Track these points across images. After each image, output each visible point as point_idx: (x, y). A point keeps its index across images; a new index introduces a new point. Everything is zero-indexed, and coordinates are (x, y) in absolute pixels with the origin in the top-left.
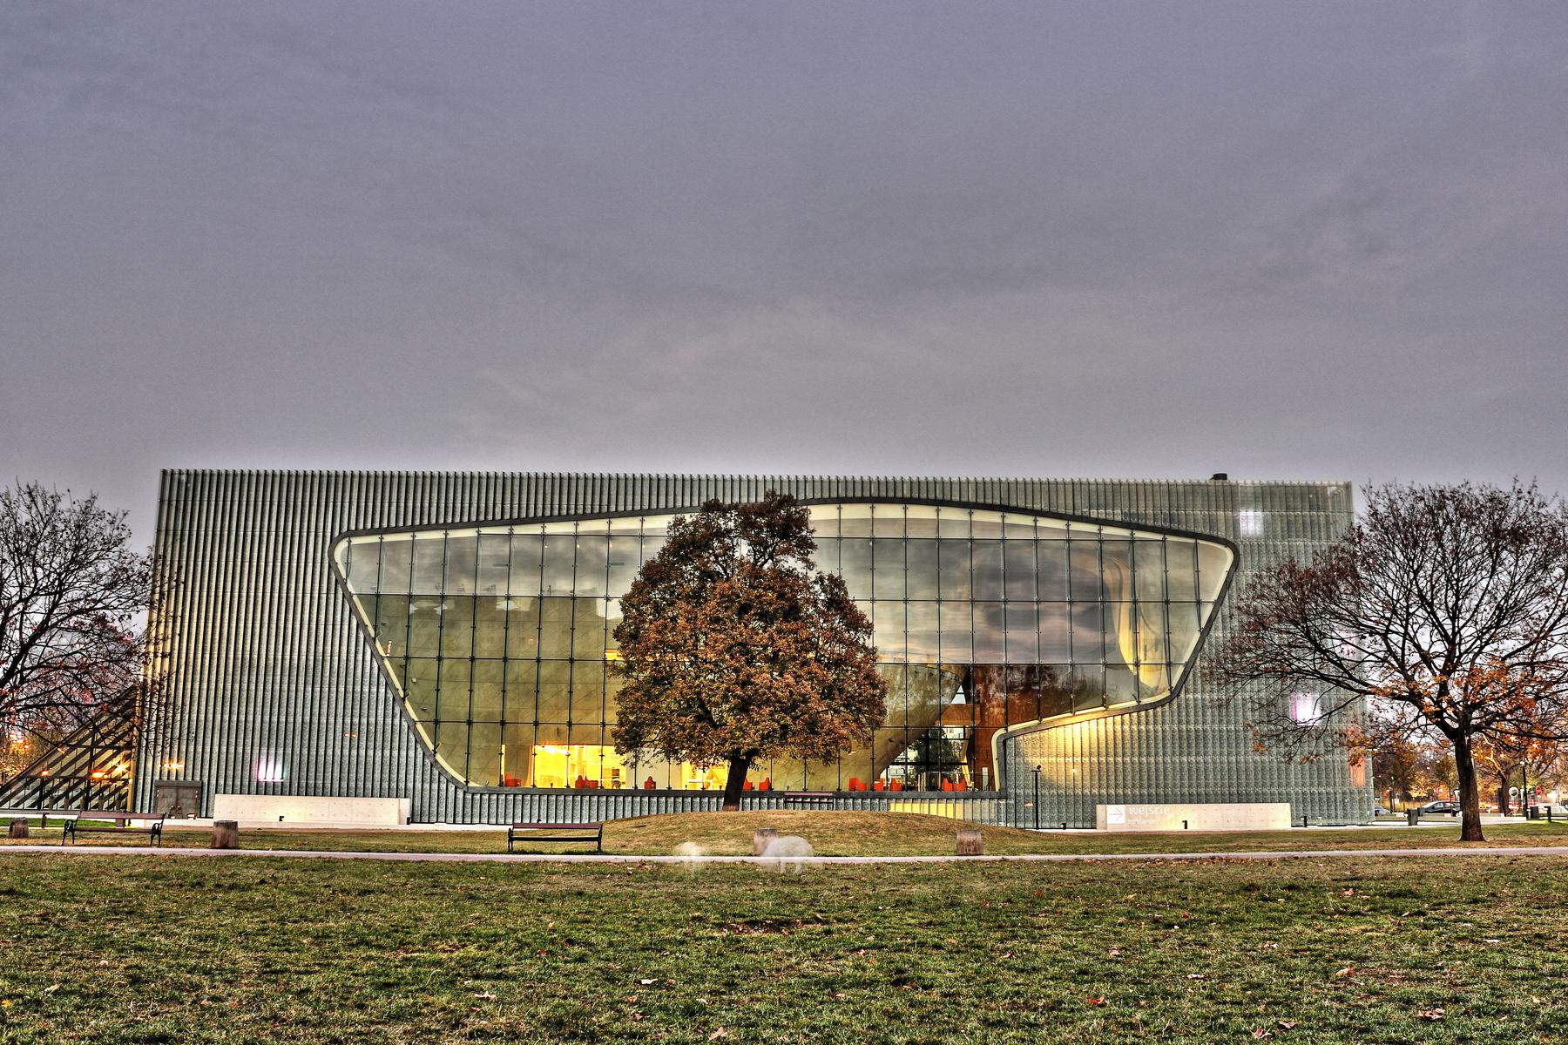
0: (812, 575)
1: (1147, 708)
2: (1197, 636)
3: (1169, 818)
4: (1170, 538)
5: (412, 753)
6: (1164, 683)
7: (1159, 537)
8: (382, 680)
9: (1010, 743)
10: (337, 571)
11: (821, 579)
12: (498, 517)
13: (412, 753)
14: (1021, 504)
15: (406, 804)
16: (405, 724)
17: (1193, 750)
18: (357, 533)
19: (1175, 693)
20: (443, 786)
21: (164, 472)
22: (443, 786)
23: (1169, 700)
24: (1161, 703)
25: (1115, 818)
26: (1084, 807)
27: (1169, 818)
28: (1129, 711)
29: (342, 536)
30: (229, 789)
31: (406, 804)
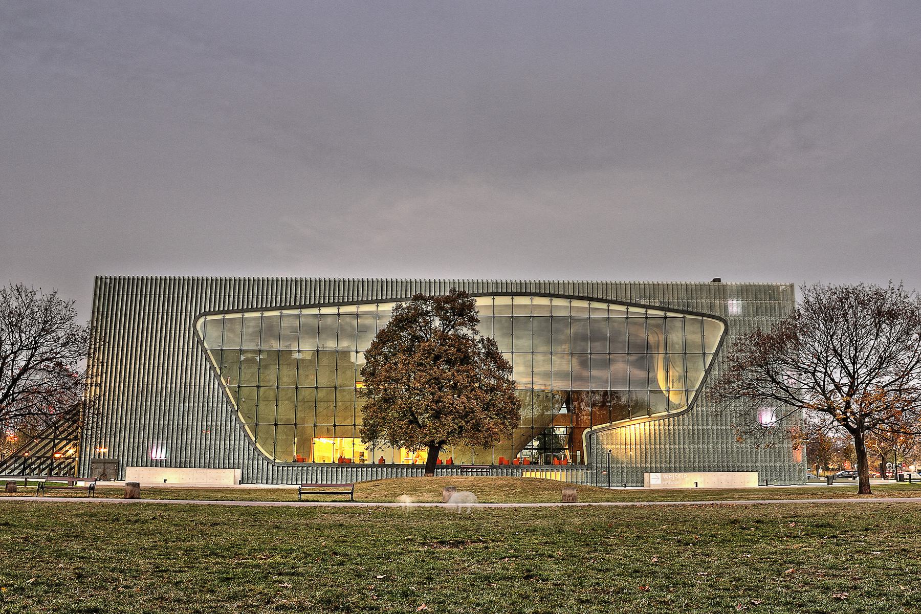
0: (477, 338)
2: (704, 373)
5: (242, 443)
6: (684, 401)
7: (681, 316)
11: (483, 340)
12: (293, 304)
14: (600, 297)
18: (210, 313)
20: (261, 462)
21: (97, 277)
22: (261, 462)
23: (687, 411)
26: (638, 477)
29: (201, 315)
31: (238, 472)
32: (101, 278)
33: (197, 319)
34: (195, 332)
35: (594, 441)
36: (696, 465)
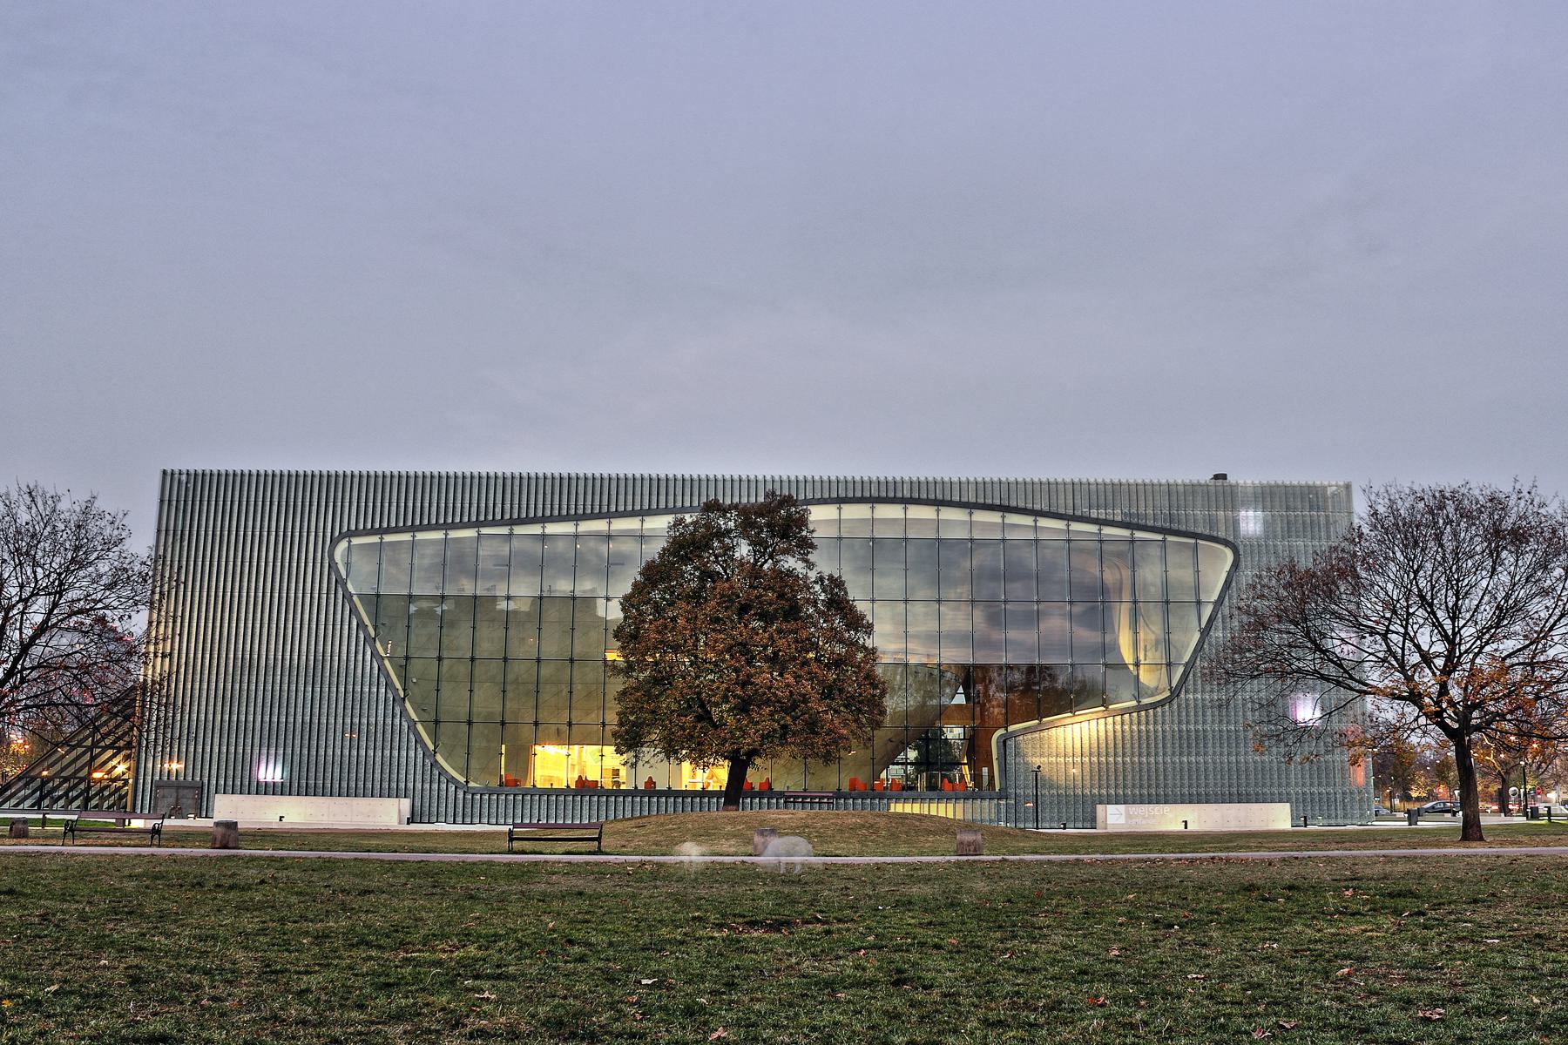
0: (813, 575)
1: (1147, 708)
2: (1197, 636)
3: (1170, 818)
4: (1170, 538)
5: (412, 753)
6: (1164, 683)
7: (1160, 537)
8: (382, 680)
9: (1010, 743)
10: (338, 571)
11: (821, 579)
12: (498, 517)
13: (412, 753)
14: (1021, 505)
15: (406, 804)
16: (405, 724)
18: (357, 533)
19: (1175, 693)
20: (444, 786)
21: (164, 472)
22: (444, 786)
23: (1169, 700)
24: (1161, 703)
25: (1115, 818)
27: (1170, 818)
28: (1129, 711)
29: (342, 536)
31: (406, 804)
33: (334, 542)
35: (1011, 751)
36: (1202, 790)
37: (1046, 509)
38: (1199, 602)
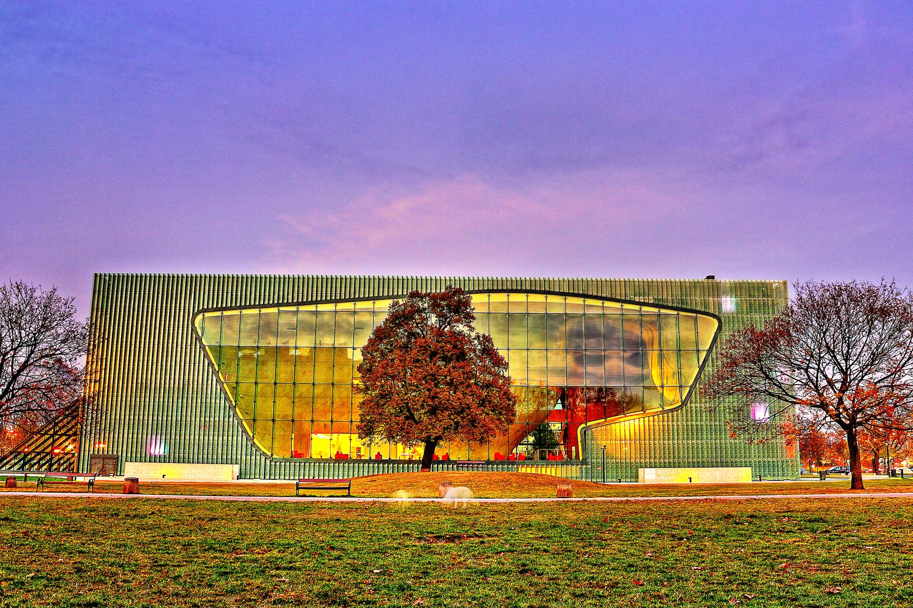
0: (473, 335)
2: (698, 369)
3: (680, 476)
5: (240, 438)
13: (240, 438)
17: (695, 437)
18: (208, 310)
20: (258, 457)
21: (96, 275)
22: (258, 457)
23: (681, 407)
24: (676, 409)
26: (633, 471)
27: (680, 476)
29: (199, 312)
30: (134, 459)
31: (236, 468)
32: (101, 275)
33: (195, 316)
34: (194, 329)
35: (589, 437)
37: (609, 296)
38: (698, 351)
